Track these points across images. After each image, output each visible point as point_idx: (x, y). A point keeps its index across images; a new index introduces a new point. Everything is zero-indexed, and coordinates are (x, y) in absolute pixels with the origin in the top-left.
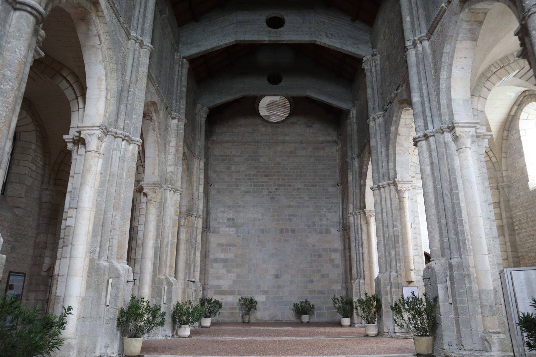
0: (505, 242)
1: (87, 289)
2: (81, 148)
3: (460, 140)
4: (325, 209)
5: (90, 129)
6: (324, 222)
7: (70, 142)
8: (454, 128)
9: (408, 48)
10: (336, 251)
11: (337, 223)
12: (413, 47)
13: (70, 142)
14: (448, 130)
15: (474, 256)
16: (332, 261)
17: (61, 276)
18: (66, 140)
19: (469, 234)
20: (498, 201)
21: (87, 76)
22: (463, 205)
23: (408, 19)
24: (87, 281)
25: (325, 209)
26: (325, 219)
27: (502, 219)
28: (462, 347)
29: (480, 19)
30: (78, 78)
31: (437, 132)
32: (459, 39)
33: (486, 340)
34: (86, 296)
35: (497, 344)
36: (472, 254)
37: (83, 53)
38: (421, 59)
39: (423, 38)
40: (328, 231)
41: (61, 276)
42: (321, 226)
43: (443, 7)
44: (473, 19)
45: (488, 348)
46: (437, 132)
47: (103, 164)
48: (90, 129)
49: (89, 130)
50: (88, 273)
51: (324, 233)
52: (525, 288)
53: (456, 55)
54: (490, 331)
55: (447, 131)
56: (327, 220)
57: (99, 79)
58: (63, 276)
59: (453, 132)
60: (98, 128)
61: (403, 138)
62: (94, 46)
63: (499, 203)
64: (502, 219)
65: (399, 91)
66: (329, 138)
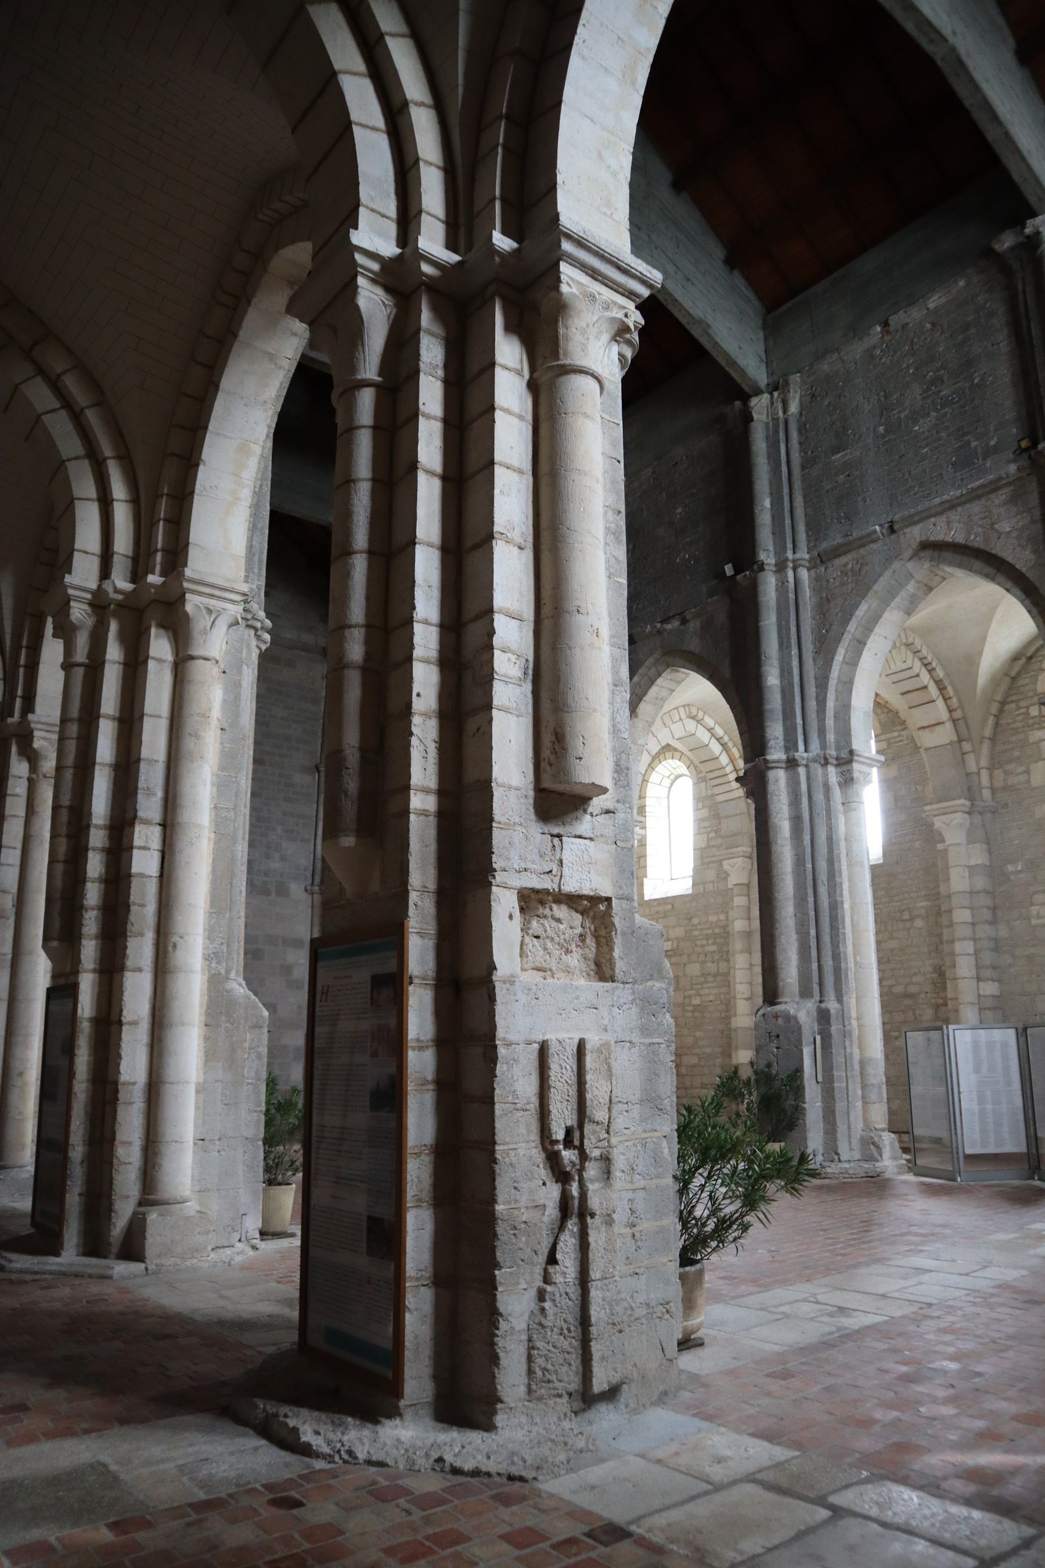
0: (751, 965)
1: (206, 1061)
2: (157, 636)
3: (855, 786)
4: (279, 830)
5: (217, 593)
6: (276, 865)
7: (79, 600)
8: (850, 761)
9: (767, 568)
10: (297, 943)
11: (306, 869)
12: (774, 569)
13: (79, 600)
14: (835, 762)
15: (857, 998)
16: (287, 969)
17: (130, 1024)
18: (70, 591)
19: (852, 960)
20: (746, 881)
21: (210, 427)
22: (847, 906)
23: (767, 503)
24: (206, 1039)
25: (279, 830)
26: (277, 856)
27: (749, 918)
28: (836, 1157)
29: (932, 584)
30: (102, 392)
31: (815, 761)
32: (892, 605)
33: (874, 1143)
34: (205, 1082)
35: (888, 1148)
36: (854, 996)
37: (230, 362)
38: (790, 605)
39: (803, 562)
40: (282, 891)
41: (130, 1024)
42: (266, 874)
43: (875, 531)
44: (925, 581)
45: (876, 1154)
46: (815, 761)
47: (224, 700)
48: (217, 593)
49: (212, 596)
50: (207, 1014)
51: (273, 894)
52: (970, 1056)
53: (877, 630)
54: (877, 1127)
55: (832, 764)
56: (283, 858)
57: (243, 450)
58: (135, 1023)
59: (845, 768)
60: (238, 598)
61: (640, 725)
62: (272, 357)
63: (748, 885)
64: (749, 918)
65: (668, 627)
66: (307, 638)
